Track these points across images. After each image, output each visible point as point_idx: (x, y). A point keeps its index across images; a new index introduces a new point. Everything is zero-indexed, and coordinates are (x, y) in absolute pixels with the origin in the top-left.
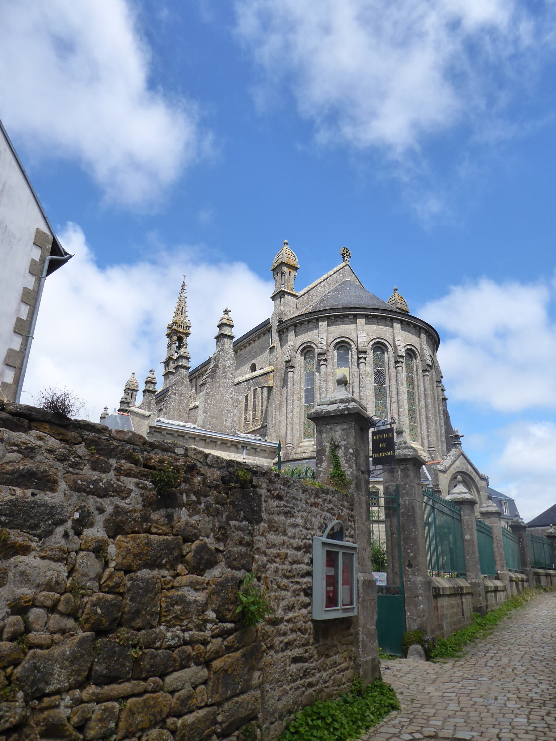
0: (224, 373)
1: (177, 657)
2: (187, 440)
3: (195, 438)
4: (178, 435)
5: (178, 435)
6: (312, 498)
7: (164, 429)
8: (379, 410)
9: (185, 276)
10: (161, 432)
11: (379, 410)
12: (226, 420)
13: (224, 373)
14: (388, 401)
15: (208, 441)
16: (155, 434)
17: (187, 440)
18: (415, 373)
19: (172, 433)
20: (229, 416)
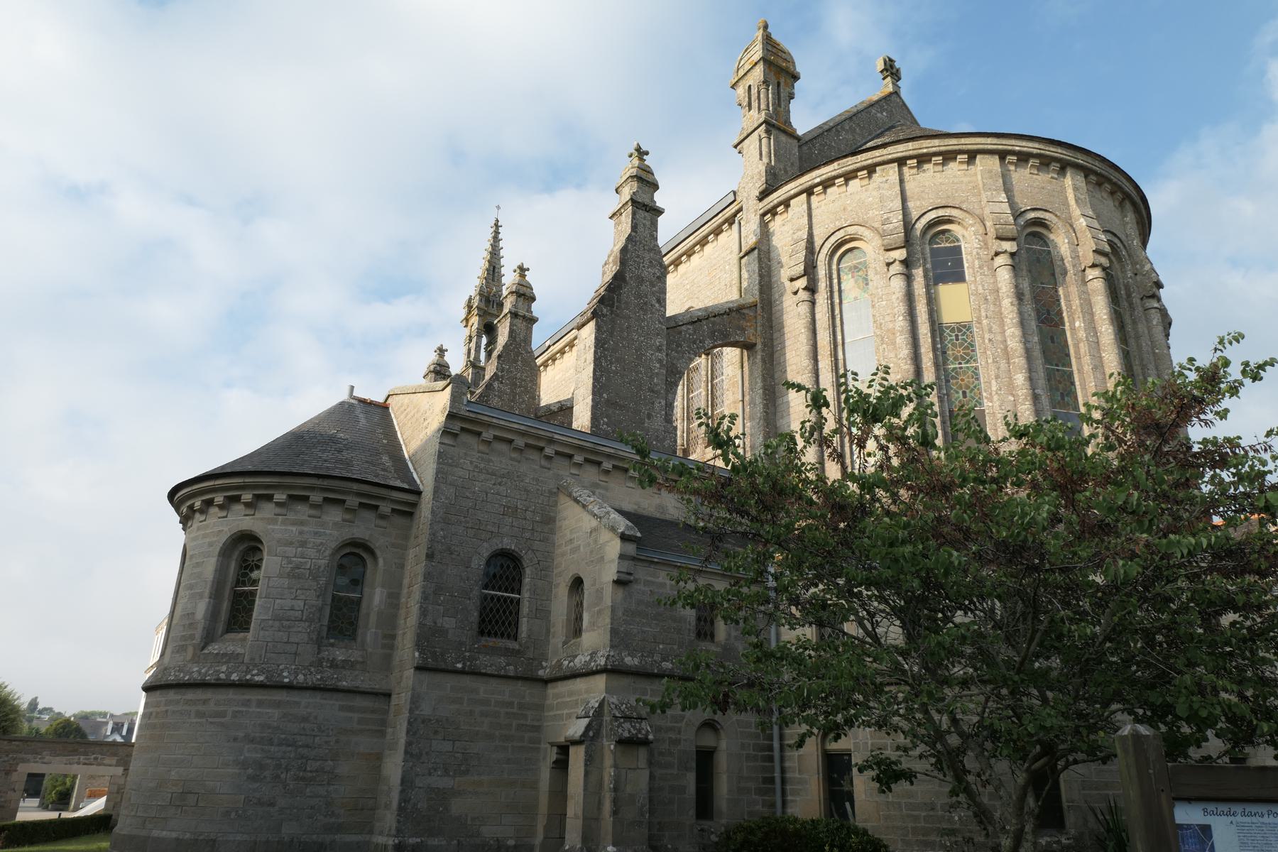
0: (639, 296)
1: (235, 557)
2: (549, 458)
3: (570, 457)
4: (527, 445)
5: (527, 445)
6: (1170, 519)
7: (489, 426)
8: (1057, 389)
9: (498, 207)
10: (479, 434)
11: (1057, 389)
12: (649, 416)
13: (639, 296)
14: (1075, 368)
15: (607, 465)
16: (465, 438)
17: (549, 458)
18: (1126, 304)
19: (510, 436)
20: (657, 405)
